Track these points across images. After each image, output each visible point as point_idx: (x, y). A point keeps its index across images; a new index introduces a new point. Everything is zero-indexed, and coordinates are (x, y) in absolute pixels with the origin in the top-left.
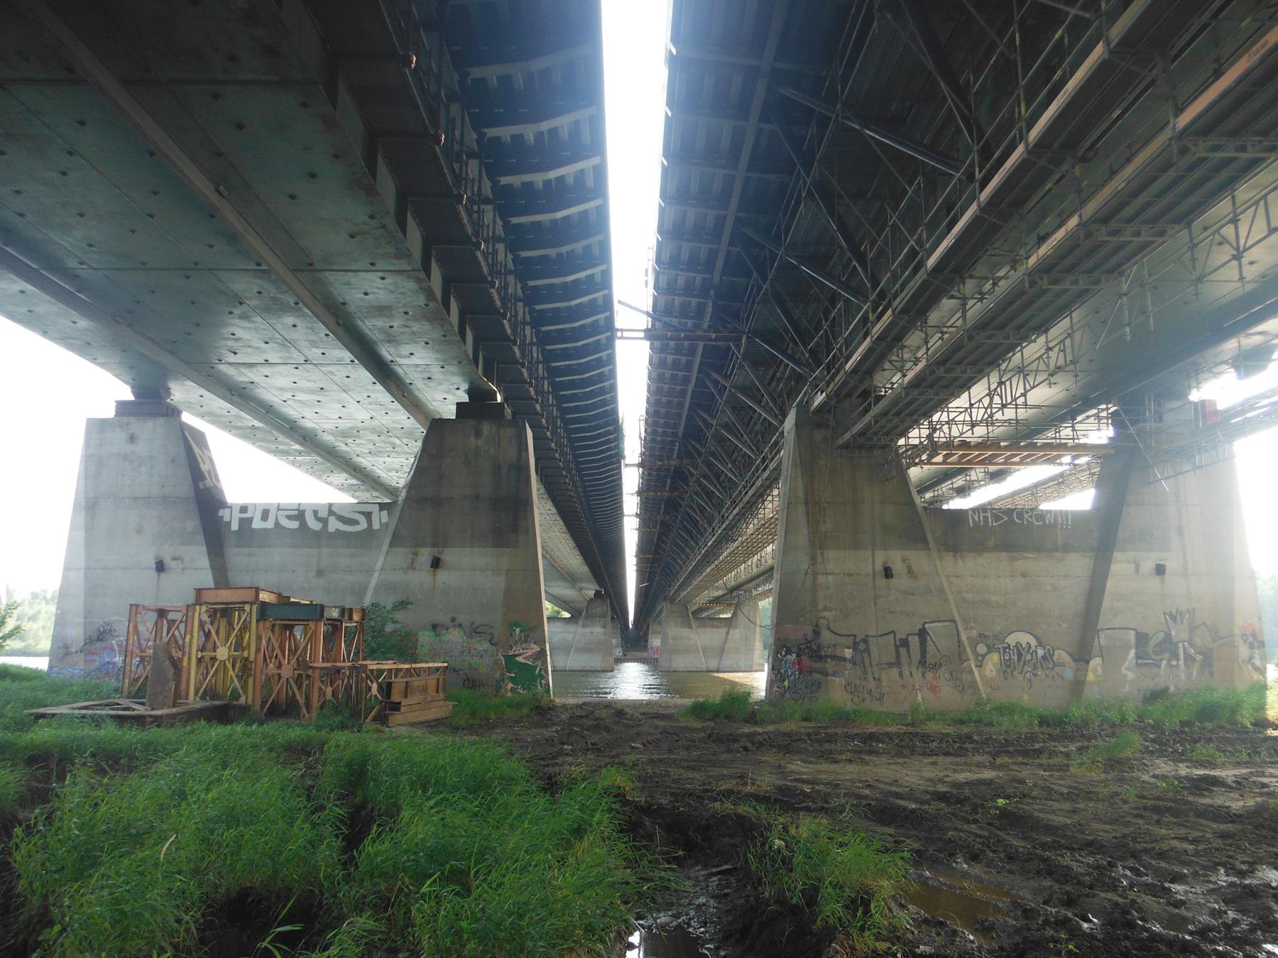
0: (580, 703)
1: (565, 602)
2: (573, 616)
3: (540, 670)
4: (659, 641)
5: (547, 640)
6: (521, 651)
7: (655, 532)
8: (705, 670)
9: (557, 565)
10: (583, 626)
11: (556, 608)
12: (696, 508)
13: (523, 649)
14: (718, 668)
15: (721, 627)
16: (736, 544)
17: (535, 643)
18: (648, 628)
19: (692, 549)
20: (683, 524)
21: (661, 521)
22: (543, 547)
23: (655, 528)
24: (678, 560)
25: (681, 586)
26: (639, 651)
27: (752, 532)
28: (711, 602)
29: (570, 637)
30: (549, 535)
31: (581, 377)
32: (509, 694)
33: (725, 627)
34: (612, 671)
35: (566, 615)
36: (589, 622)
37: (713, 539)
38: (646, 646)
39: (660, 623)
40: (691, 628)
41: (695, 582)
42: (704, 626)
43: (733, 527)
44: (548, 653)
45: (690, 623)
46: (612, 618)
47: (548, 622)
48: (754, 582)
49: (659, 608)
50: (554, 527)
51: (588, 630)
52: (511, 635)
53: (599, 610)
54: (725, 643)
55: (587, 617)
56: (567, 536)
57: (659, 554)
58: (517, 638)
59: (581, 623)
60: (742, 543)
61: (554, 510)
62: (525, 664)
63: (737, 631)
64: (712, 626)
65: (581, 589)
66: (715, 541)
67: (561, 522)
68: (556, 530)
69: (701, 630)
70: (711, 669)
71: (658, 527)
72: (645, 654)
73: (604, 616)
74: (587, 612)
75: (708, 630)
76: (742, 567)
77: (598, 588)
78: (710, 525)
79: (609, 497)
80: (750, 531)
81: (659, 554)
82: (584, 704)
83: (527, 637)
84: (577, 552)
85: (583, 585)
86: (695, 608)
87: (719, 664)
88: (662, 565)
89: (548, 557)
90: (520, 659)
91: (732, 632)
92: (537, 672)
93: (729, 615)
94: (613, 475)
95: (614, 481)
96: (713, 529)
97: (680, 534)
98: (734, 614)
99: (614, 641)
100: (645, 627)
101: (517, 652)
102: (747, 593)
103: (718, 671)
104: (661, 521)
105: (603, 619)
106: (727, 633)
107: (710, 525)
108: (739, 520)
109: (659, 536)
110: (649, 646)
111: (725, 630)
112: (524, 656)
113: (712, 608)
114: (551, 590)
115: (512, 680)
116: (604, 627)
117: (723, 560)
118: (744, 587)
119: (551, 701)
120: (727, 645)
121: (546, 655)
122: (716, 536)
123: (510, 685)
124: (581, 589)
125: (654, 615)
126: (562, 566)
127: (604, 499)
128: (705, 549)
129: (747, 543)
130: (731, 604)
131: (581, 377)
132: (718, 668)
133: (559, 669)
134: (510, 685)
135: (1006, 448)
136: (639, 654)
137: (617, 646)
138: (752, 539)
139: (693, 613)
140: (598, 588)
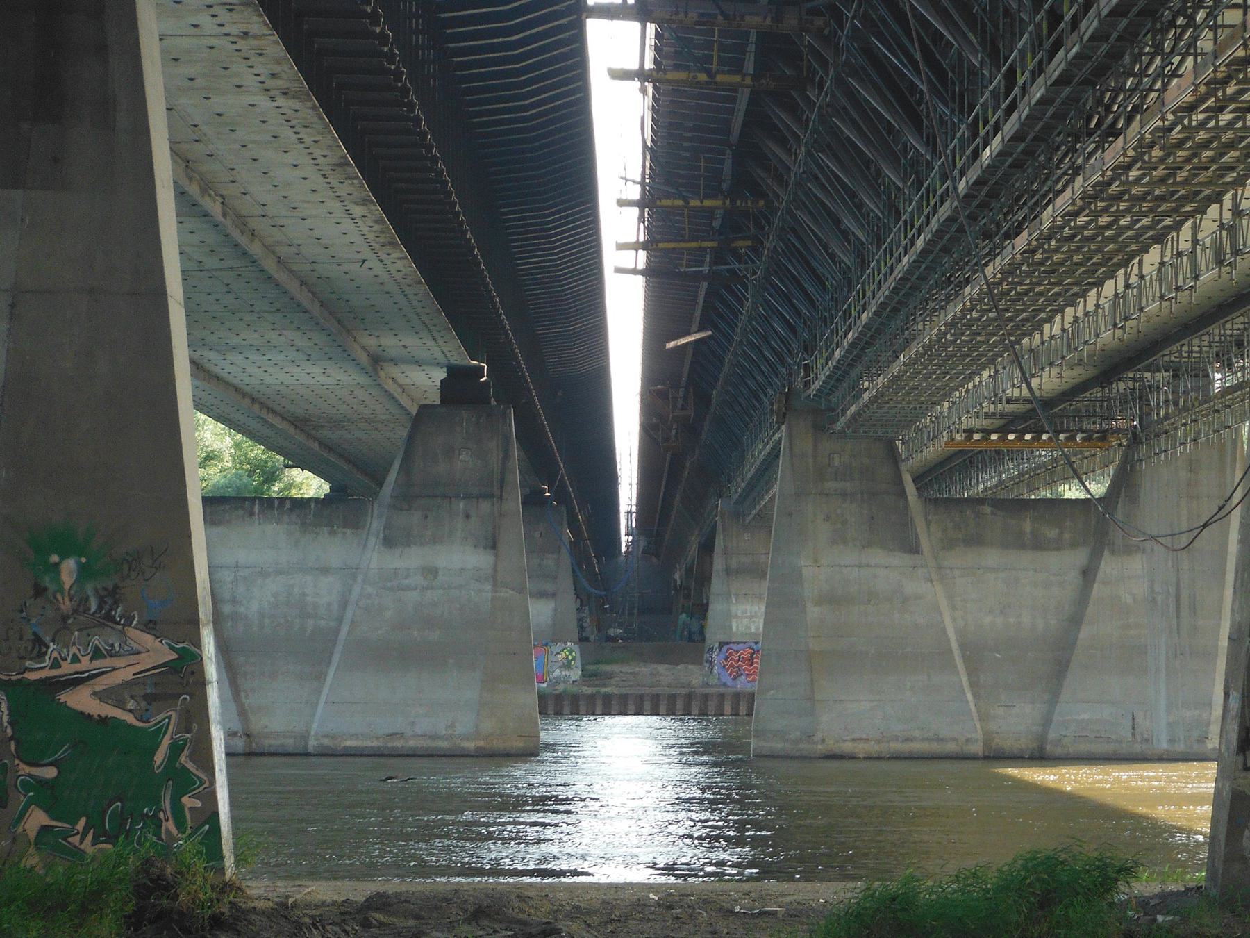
0: (360, 899)
1: (300, 423)
2: (339, 494)
3: (176, 749)
4: (759, 609)
5: (205, 610)
6: (85, 663)
7: (733, 88)
8: (977, 748)
9: (255, 249)
10: (389, 542)
11: (258, 451)
12: (918, 57)
13: (97, 654)
14: (1042, 739)
15: (1057, 546)
16: (1114, 153)
17: (150, 626)
18: (707, 547)
19: (915, 170)
20: (869, 53)
21: (763, 36)
22: (183, 160)
23: (736, 66)
24: (848, 222)
25: (859, 348)
26: (663, 657)
27: (1188, 98)
28: (1009, 423)
29: (324, 591)
30: (217, 102)
31: (523, 103)
32: (33, 860)
33: (1073, 545)
34: (530, 752)
35: (311, 485)
36: (416, 516)
37: (1011, 126)
38: (697, 637)
39: (763, 521)
40: (914, 549)
41: (929, 331)
42: (976, 541)
43: (1100, 72)
44: (212, 670)
45: (905, 523)
46: (532, 501)
47: (209, 520)
48: (1215, 330)
49: (760, 452)
50: (239, 67)
51: (411, 559)
52: (39, 591)
53: (465, 462)
54: (1076, 620)
55: (407, 498)
56: (308, 110)
57: (758, 193)
58: (66, 605)
59: (376, 524)
60: (1144, 147)
61: (289, 71)
62: (103, 721)
63: (1136, 564)
64: (1017, 543)
65: (377, 360)
66: (1017, 138)
67: (275, 47)
68: (250, 81)
69: (959, 559)
70: (1007, 743)
71: (749, 67)
72: (691, 676)
73: (491, 490)
74: (405, 468)
75: (992, 557)
76: (1153, 257)
77: (460, 357)
78: (995, 56)
79: (582, 279)
80: (1180, 92)
81: (758, 193)
82: (380, 902)
83: (111, 596)
84: (355, 187)
85: (389, 343)
86: (930, 453)
87: (1047, 722)
88: (770, 243)
89: (215, 209)
90: (81, 700)
91: (1109, 566)
92: (160, 757)
93: (1098, 489)
94: (592, 241)
95: (565, 57)
96: (1011, 76)
97: (852, 95)
98: (1124, 483)
99: (541, 612)
100: (693, 549)
101: (67, 668)
102: (1186, 383)
103: (1040, 757)
104: (763, 36)
105: (485, 506)
106: (1088, 574)
107: (995, 56)
108: (1130, 37)
109: (754, 101)
110: (713, 636)
111: (1076, 558)
112: (101, 684)
113: (1017, 452)
114: (230, 366)
115: (47, 794)
116: (493, 544)
117: (1055, 229)
118: (1171, 354)
119: (226, 888)
120: (1085, 632)
121: (202, 684)
122: (1023, 111)
123: (37, 819)
124: (377, 360)
125: (738, 487)
126: (283, 251)
127: (554, 248)
128: (973, 174)
129: (1170, 150)
130: (1104, 435)
131: (523, 103)
132: (1042, 739)
133: (268, 743)
134: (37, 819)
135: (798, 880)
136: (666, 675)
137: (555, 636)
138: (1190, 131)
139: (927, 477)
140: (460, 357)
